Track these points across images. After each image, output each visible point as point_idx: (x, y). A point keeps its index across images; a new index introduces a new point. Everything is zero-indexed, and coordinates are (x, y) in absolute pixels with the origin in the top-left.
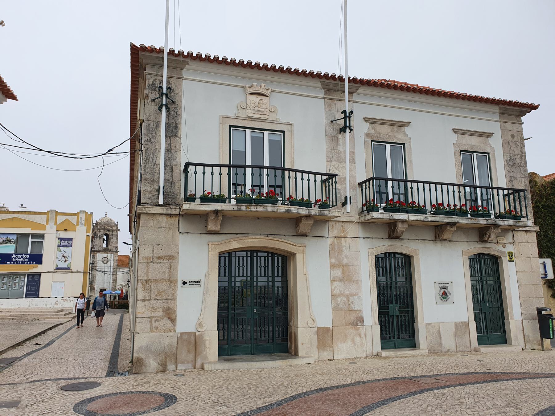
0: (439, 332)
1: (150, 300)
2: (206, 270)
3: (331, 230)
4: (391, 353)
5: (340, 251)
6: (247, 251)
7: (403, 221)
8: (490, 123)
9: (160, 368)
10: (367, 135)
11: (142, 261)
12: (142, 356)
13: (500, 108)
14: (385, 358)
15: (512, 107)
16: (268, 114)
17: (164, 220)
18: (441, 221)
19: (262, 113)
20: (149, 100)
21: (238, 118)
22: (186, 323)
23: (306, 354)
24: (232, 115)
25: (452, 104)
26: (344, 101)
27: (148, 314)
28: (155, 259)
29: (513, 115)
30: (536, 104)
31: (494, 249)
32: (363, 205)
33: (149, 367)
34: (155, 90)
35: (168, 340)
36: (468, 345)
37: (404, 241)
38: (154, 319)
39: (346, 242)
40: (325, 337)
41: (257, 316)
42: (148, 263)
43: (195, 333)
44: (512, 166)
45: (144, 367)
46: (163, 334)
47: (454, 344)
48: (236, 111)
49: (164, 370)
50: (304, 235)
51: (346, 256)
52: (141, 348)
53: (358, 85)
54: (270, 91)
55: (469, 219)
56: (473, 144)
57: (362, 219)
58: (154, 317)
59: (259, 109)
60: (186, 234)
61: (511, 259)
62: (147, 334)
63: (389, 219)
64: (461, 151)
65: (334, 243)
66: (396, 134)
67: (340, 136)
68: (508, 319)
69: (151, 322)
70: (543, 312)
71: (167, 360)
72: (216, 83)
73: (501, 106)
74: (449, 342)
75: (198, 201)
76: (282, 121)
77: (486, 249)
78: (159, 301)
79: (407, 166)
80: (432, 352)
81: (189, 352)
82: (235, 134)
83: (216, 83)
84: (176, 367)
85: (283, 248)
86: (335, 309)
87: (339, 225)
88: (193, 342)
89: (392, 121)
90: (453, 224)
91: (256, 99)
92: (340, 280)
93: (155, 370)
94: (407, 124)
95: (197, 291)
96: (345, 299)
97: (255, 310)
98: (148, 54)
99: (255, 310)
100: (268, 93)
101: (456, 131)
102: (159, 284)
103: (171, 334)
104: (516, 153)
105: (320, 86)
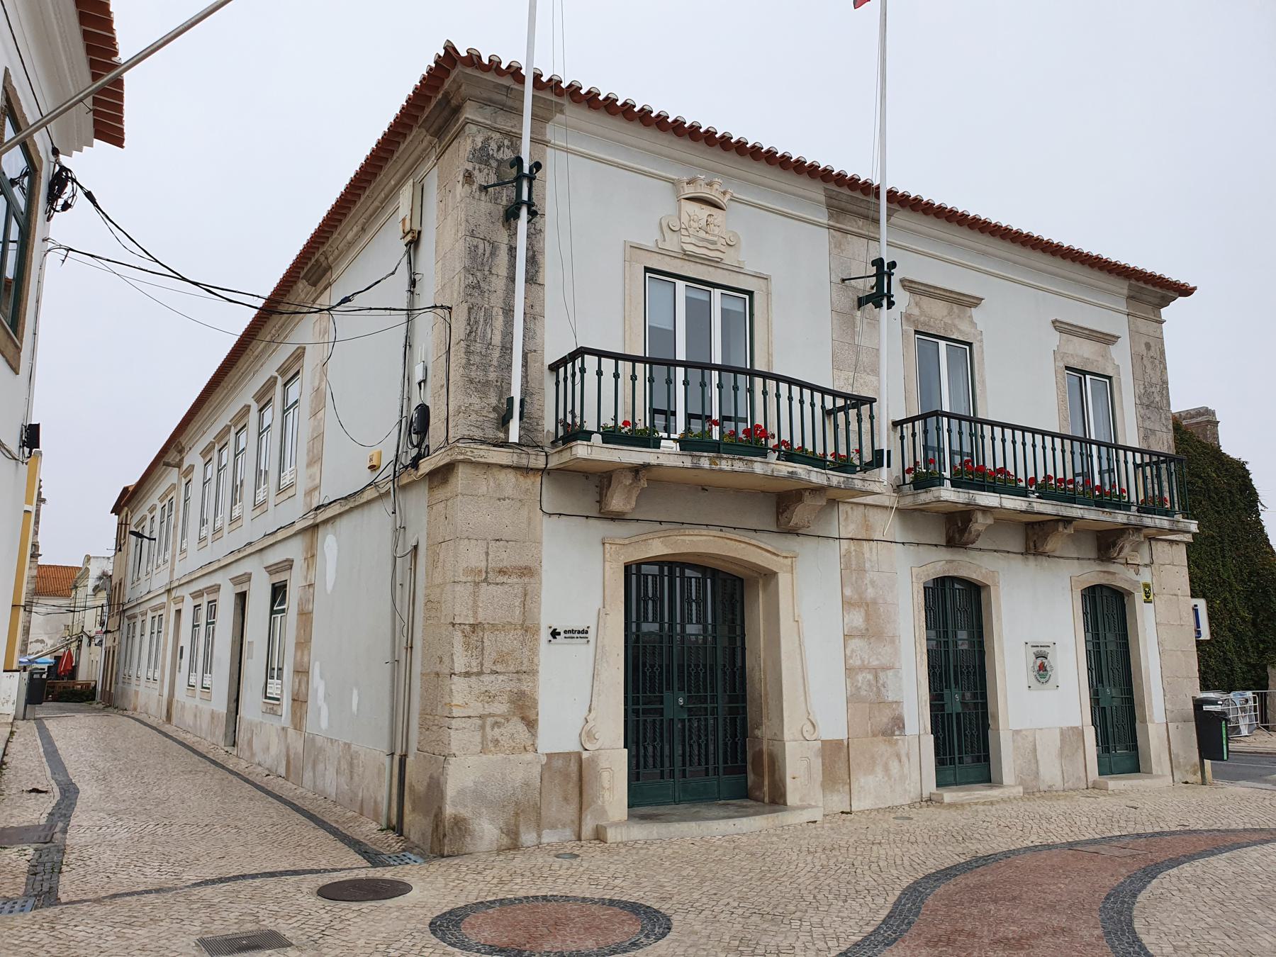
0: (1035, 749)
1: (480, 673)
2: (599, 604)
3: (847, 522)
4: (961, 794)
5: (861, 570)
7: (986, 510)
8: (1106, 312)
9: (506, 841)
11: (463, 579)
12: (465, 812)
13: (1130, 285)
14: (950, 805)
15: (1150, 287)
16: (722, 248)
17: (509, 480)
18: (1054, 512)
19: (711, 247)
20: (475, 187)
21: (662, 253)
22: (558, 730)
23: (801, 800)
24: (650, 244)
25: (1050, 268)
26: (878, 240)
27: (477, 708)
28: (491, 575)
29: (1149, 303)
30: (1192, 286)
31: (1121, 576)
32: (905, 472)
33: (481, 838)
34: (487, 164)
35: (522, 771)
36: (1082, 775)
37: (973, 553)
38: (490, 721)
39: (871, 549)
40: (836, 761)
41: (697, 716)
42: (477, 584)
43: (579, 754)
44: (1148, 406)
45: (468, 839)
46: (511, 757)
47: (1059, 773)
48: (658, 236)
49: (515, 846)
50: (794, 532)
51: (872, 582)
52: (462, 792)
54: (728, 196)
55: (1078, 513)
56: (1086, 355)
57: (908, 502)
58: (490, 715)
59: (707, 236)
60: (556, 517)
62: (476, 758)
63: (967, 504)
64: (1067, 368)
66: (957, 322)
67: (859, 313)
68: (1144, 721)
69: (483, 727)
70: (1206, 708)
71: (519, 818)
72: (618, 166)
73: (1133, 282)
74: (1051, 772)
75: (597, 439)
76: (749, 268)
77: (1110, 577)
78: (501, 677)
79: (978, 391)
80: (1032, 792)
81: (566, 799)
82: (659, 290)
83: (618, 166)
84: (539, 836)
85: (753, 560)
87: (857, 513)
88: (575, 776)
89: (951, 292)
90: (1068, 521)
91: (702, 212)
92: (862, 636)
93: (495, 846)
94: (975, 302)
95: (580, 652)
96: (870, 677)
97: (681, 701)
98: (477, 73)
99: (681, 701)
100: (724, 201)
101: (1058, 325)
102: (501, 636)
103: (529, 756)
104: (1154, 381)
105: (823, 198)
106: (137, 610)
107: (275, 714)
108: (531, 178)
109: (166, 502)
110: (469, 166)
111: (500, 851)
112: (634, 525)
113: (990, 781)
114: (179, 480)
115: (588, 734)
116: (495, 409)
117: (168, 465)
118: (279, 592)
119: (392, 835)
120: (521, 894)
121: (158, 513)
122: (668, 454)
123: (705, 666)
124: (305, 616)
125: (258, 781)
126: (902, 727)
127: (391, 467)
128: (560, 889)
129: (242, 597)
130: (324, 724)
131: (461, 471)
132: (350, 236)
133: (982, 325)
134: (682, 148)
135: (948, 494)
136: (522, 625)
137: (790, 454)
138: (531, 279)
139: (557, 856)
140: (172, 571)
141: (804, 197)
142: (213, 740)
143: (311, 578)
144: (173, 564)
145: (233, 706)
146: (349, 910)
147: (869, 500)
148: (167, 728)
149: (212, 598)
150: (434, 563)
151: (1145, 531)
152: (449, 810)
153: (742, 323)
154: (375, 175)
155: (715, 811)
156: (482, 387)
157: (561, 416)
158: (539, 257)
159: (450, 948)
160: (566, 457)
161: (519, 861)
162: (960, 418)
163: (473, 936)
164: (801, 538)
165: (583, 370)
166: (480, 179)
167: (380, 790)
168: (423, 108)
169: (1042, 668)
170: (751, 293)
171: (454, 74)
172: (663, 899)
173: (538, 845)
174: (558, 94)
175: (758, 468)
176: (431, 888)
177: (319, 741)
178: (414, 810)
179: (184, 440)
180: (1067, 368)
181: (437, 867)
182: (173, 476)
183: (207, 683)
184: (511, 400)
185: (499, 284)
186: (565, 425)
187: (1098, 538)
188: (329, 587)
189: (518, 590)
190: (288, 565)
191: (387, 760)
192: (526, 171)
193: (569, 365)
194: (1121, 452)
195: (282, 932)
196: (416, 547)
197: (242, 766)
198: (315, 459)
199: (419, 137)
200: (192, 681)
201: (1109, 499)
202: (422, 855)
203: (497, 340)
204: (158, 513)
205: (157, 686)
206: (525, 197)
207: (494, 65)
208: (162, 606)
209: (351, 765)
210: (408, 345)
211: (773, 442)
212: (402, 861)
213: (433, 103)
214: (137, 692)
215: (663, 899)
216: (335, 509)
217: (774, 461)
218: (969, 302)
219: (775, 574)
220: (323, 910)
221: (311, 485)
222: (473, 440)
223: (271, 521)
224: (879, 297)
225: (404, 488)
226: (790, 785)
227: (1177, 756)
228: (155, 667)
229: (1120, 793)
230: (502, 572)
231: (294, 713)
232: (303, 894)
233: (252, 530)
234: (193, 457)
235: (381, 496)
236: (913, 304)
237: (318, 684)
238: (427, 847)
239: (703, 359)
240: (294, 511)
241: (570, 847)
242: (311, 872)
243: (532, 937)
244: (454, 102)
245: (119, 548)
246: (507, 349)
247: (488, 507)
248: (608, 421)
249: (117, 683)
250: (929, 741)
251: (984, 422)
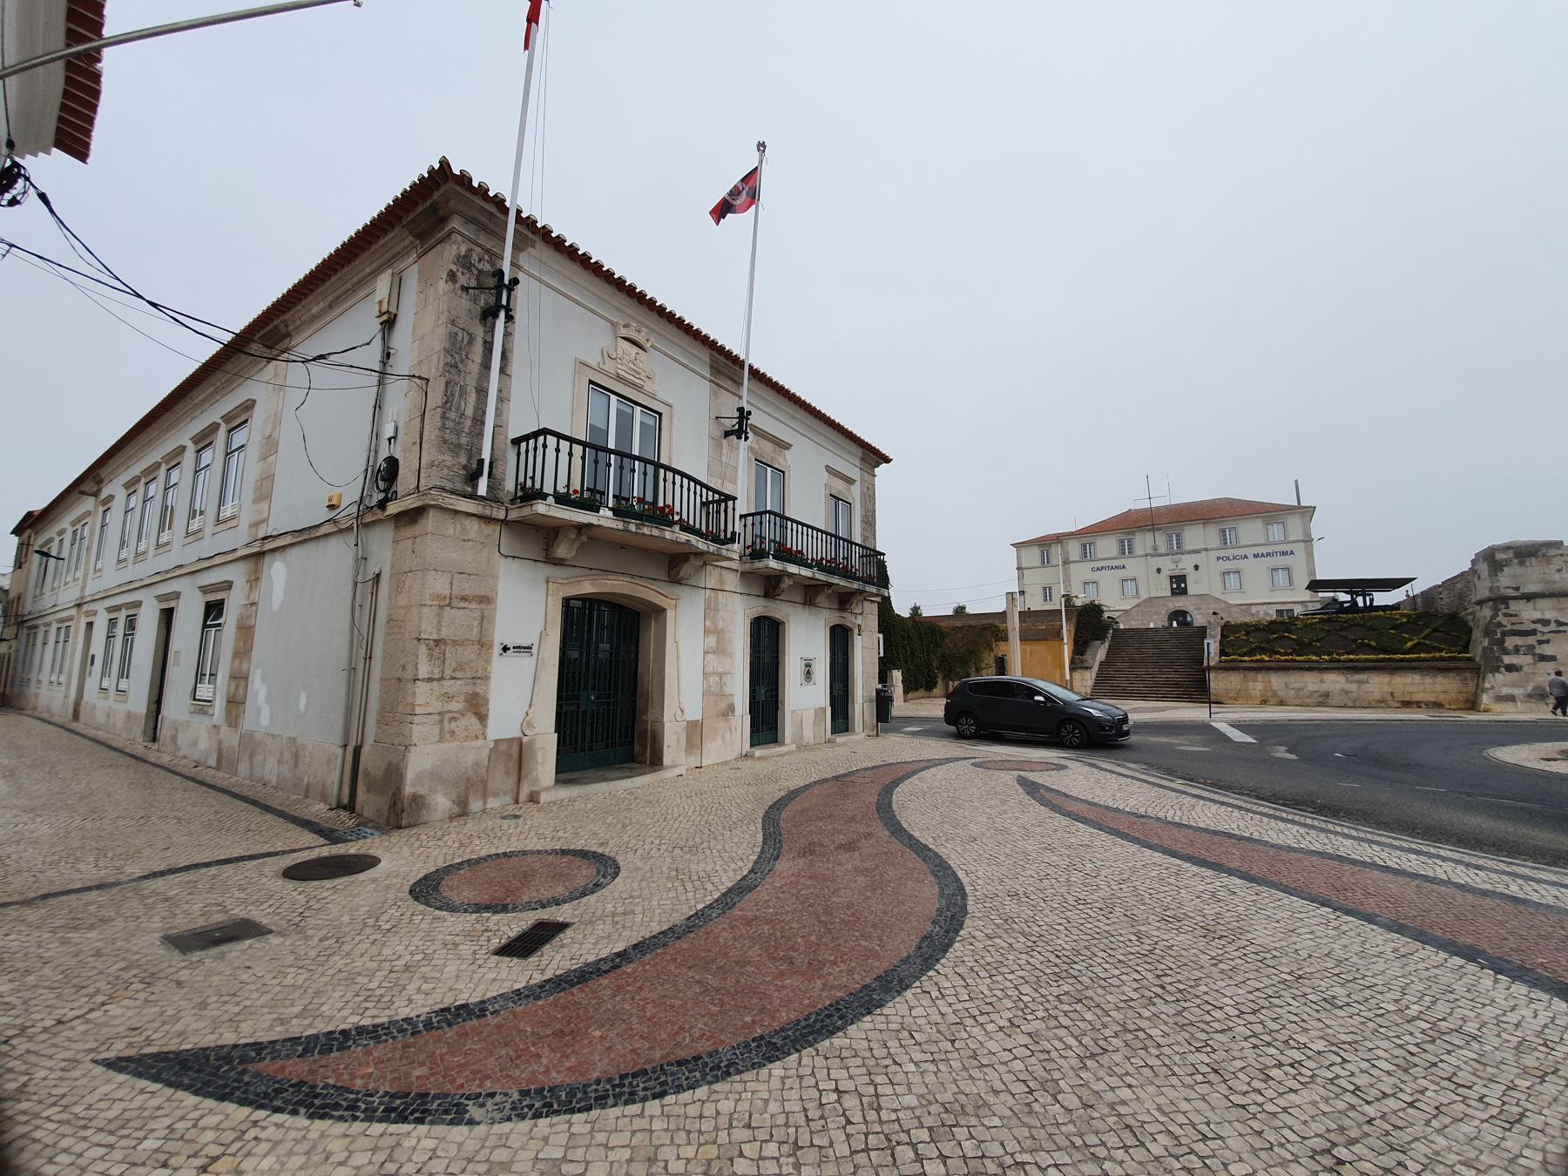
3: (711, 578)
5: (717, 609)
7: (791, 575)
9: (456, 810)
12: (420, 790)
14: (760, 758)
17: (474, 526)
21: (602, 372)
22: (504, 721)
24: (594, 365)
27: (437, 706)
32: (746, 547)
34: (469, 269)
35: (473, 754)
38: (447, 717)
40: (695, 733)
52: (420, 775)
57: (747, 567)
69: (441, 721)
71: (468, 793)
75: (551, 500)
80: (801, 747)
81: (507, 773)
82: (598, 399)
87: (716, 572)
88: (516, 756)
90: (830, 585)
94: (787, 446)
95: (526, 663)
98: (467, 194)
101: (829, 469)
103: (480, 743)
106: (39, 622)
107: (205, 713)
108: (510, 290)
109: (79, 526)
110: (454, 268)
111: (451, 819)
114: (96, 508)
115: (527, 723)
116: (464, 467)
117: (84, 493)
118: (214, 610)
119: (343, 814)
120: (484, 853)
121: (68, 537)
122: (604, 518)
124: (246, 630)
125: (185, 771)
126: (733, 711)
127: (355, 509)
128: (514, 846)
129: (168, 616)
130: (265, 720)
131: (432, 514)
132: (315, 310)
134: (620, 300)
135: (773, 564)
137: (686, 528)
138: (503, 371)
139: (504, 818)
140: (83, 588)
142: (135, 739)
143: (254, 597)
144: (85, 581)
145: (154, 707)
146: (323, 889)
147: (724, 564)
148: (74, 726)
149: (131, 612)
150: (398, 588)
152: (408, 790)
153: (655, 433)
154: (350, 261)
155: (615, 774)
156: (455, 448)
157: (521, 479)
159: (437, 912)
160: (526, 512)
161: (471, 826)
162: (776, 515)
163: (455, 898)
165: (545, 446)
166: (463, 280)
167: (333, 778)
168: (417, 204)
169: (808, 673)
171: (443, 189)
172: (602, 845)
173: (484, 811)
174: (533, 233)
175: (668, 535)
176: (400, 859)
177: (258, 737)
178: (368, 791)
179: (103, 473)
181: (396, 837)
182: (88, 504)
183: (123, 685)
184: (481, 462)
185: (474, 368)
186: (523, 488)
188: (276, 604)
189: (477, 614)
190: (228, 585)
191: (340, 751)
195: (258, 920)
196: (378, 575)
197: (165, 759)
198: (264, 494)
199: (399, 237)
200: (105, 684)
201: (847, 573)
202: (377, 828)
203: (469, 412)
204: (68, 537)
205: (63, 688)
206: (504, 302)
207: (482, 191)
208: (71, 619)
209: (296, 756)
210: (378, 406)
211: (677, 518)
212: (360, 837)
213: (420, 209)
214: (37, 695)
215: (602, 845)
216: (288, 540)
218: (783, 446)
219: (664, 610)
220: (296, 892)
221: (256, 518)
222: (443, 489)
223: (207, 547)
224: (740, 432)
225: (366, 525)
226: (666, 751)
228: (61, 672)
229: (843, 744)
230: (464, 599)
231: (228, 713)
232: (268, 878)
233: (187, 554)
234: (114, 487)
235: (341, 531)
237: (258, 687)
238: (383, 821)
240: (238, 539)
241: (511, 810)
242: (269, 855)
243: (509, 892)
244: (441, 212)
245: (19, 564)
246: (479, 421)
247: (453, 547)
248: (561, 489)
249: (12, 685)
250: (748, 718)
251: (788, 519)
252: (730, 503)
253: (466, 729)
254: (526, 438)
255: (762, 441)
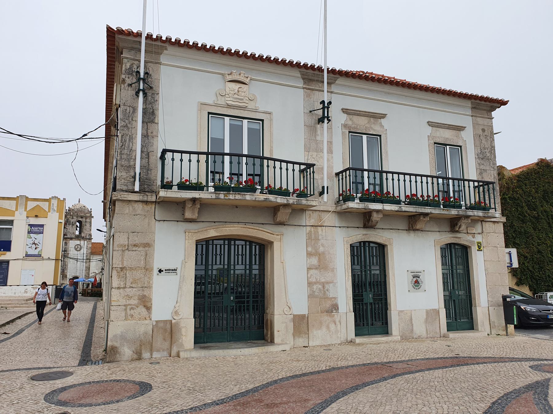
0: (411, 319)
1: (125, 288)
3: (309, 219)
4: (365, 339)
5: (317, 239)
6: (224, 240)
7: (378, 211)
8: (462, 116)
9: (135, 356)
10: (345, 126)
12: (116, 344)
13: (472, 103)
14: (359, 344)
15: (483, 102)
16: (247, 102)
17: (139, 207)
18: (414, 211)
20: (126, 85)
21: (216, 105)
23: (281, 341)
24: (211, 102)
25: (426, 98)
27: (123, 302)
28: (130, 247)
29: (485, 110)
30: (506, 100)
31: (464, 239)
32: (340, 195)
33: (124, 355)
34: (132, 74)
35: (143, 328)
36: (438, 331)
38: (129, 307)
39: (322, 230)
40: (301, 324)
41: (233, 303)
42: (123, 251)
43: (171, 321)
44: (482, 159)
45: (118, 355)
46: (139, 322)
48: (214, 98)
49: (140, 358)
50: (282, 224)
51: (323, 245)
52: (115, 336)
53: (337, 76)
54: (249, 79)
55: (440, 210)
56: (447, 137)
57: (339, 209)
58: (129, 305)
60: (162, 222)
61: (479, 249)
62: (122, 322)
63: (364, 209)
64: (435, 143)
65: (310, 231)
66: (372, 126)
67: (319, 126)
69: (126, 310)
73: (473, 101)
74: (420, 329)
75: (175, 188)
76: (261, 109)
77: (457, 239)
78: (134, 289)
79: (383, 157)
80: (405, 338)
81: (164, 339)
82: (214, 121)
84: (151, 355)
86: (311, 296)
88: (169, 330)
89: (369, 112)
92: (316, 268)
93: (130, 359)
94: (383, 116)
96: (320, 286)
97: (232, 298)
98: (154, 43)
99: (232, 298)
100: (247, 81)
101: (430, 124)
102: (135, 272)
103: (147, 322)
104: (486, 146)
105: (300, 75)
108: (328, 108)
111: (132, 360)
112: (201, 224)
113: (388, 333)
123: (380, 282)
133: (389, 128)
136: (145, 268)
141: (424, 99)
151: (471, 218)
158: (155, 111)
160: (344, 207)
164: (285, 227)
169: (417, 282)
170: (262, 121)
180: (435, 143)
184: (323, 187)
187: (451, 222)
189: (143, 253)
192: (326, 105)
193: (308, 170)
194: (466, 183)
206: (326, 115)
207: (312, 67)
217: (259, 194)
218: (378, 117)
219: (273, 242)
226: (276, 333)
227: (494, 322)
236: (348, 119)
239: (238, 152)
252: (491, 186)
253: (139, 314)
254: (342, 172)
255: (355, 118)
